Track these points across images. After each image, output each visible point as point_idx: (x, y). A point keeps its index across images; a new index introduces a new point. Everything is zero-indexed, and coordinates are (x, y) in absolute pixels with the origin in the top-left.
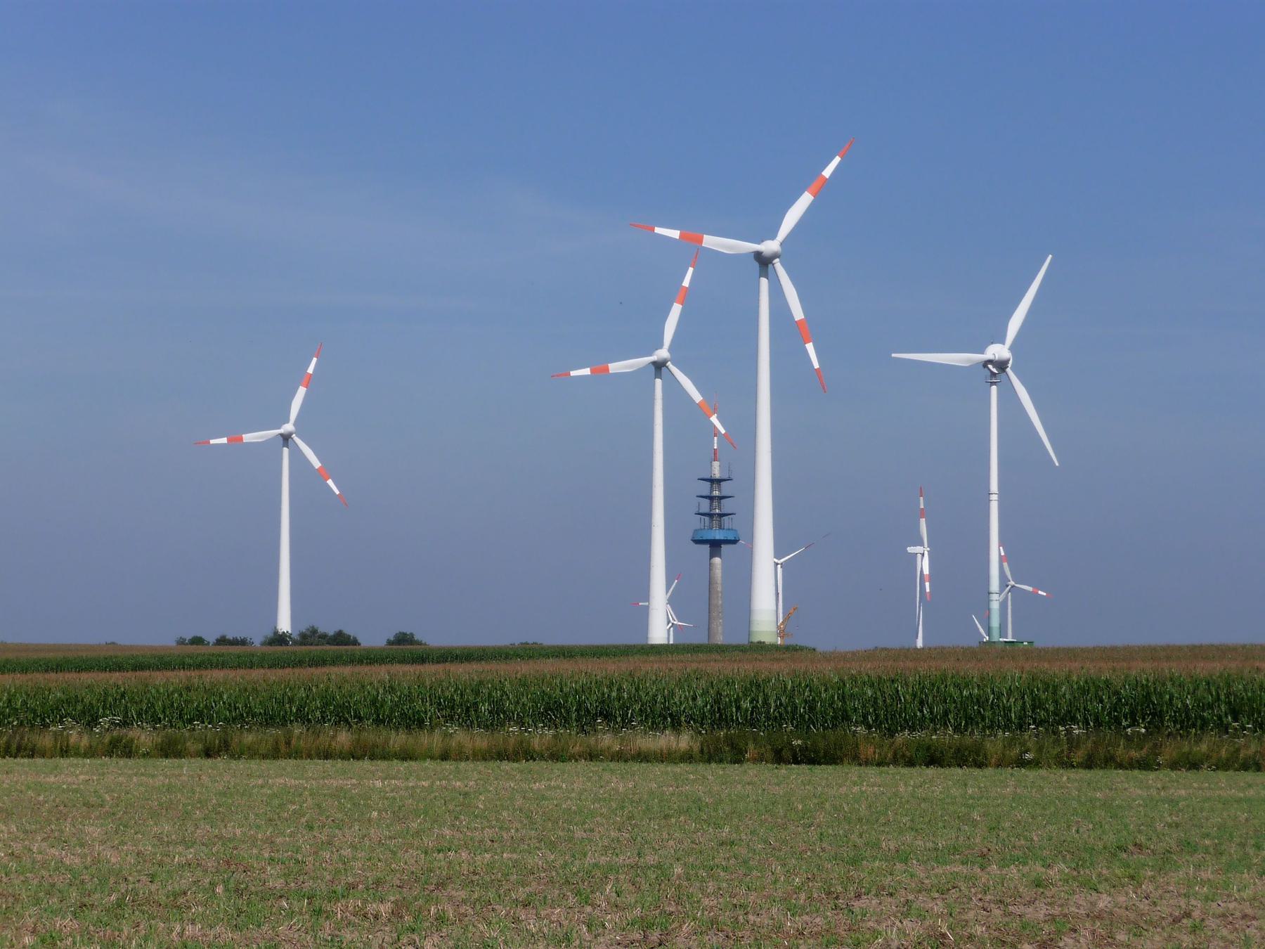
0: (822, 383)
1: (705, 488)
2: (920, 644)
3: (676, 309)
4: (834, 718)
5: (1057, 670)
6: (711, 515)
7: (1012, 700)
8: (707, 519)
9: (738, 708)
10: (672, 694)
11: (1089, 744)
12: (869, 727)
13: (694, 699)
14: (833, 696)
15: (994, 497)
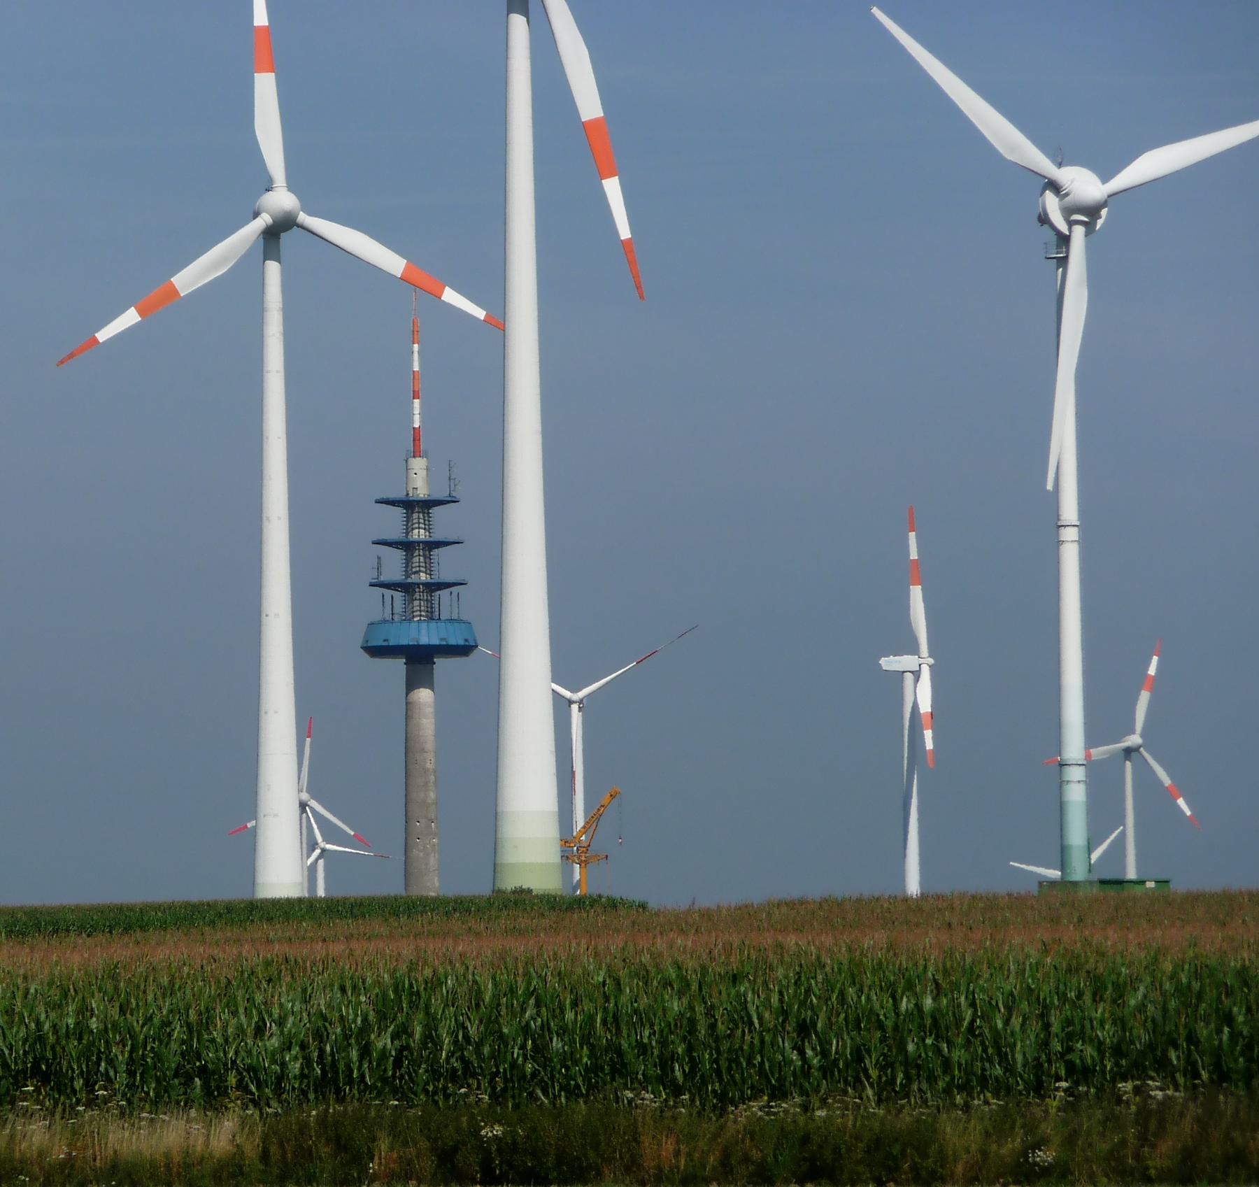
0: (636, 277)
1: (392, 523)
2: (913, 886)
3: (265, 86)
4: (595, 1069)
5: (1124, 946)
6: (406, 588)
7: (1016, 1022)
8: (398, 596)
9: (365, 1051)
10: (207, 1021)
11: (1187, 1125)
12: (677, 1091)
13: (260, 1031)
14: (591, 1018)
15: (1070, 535)
